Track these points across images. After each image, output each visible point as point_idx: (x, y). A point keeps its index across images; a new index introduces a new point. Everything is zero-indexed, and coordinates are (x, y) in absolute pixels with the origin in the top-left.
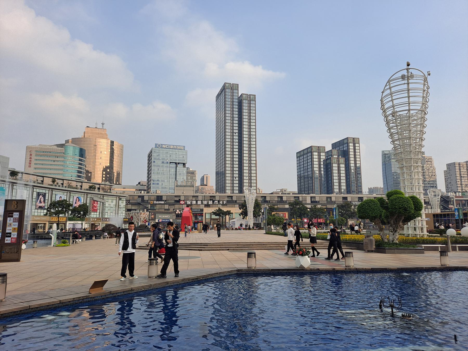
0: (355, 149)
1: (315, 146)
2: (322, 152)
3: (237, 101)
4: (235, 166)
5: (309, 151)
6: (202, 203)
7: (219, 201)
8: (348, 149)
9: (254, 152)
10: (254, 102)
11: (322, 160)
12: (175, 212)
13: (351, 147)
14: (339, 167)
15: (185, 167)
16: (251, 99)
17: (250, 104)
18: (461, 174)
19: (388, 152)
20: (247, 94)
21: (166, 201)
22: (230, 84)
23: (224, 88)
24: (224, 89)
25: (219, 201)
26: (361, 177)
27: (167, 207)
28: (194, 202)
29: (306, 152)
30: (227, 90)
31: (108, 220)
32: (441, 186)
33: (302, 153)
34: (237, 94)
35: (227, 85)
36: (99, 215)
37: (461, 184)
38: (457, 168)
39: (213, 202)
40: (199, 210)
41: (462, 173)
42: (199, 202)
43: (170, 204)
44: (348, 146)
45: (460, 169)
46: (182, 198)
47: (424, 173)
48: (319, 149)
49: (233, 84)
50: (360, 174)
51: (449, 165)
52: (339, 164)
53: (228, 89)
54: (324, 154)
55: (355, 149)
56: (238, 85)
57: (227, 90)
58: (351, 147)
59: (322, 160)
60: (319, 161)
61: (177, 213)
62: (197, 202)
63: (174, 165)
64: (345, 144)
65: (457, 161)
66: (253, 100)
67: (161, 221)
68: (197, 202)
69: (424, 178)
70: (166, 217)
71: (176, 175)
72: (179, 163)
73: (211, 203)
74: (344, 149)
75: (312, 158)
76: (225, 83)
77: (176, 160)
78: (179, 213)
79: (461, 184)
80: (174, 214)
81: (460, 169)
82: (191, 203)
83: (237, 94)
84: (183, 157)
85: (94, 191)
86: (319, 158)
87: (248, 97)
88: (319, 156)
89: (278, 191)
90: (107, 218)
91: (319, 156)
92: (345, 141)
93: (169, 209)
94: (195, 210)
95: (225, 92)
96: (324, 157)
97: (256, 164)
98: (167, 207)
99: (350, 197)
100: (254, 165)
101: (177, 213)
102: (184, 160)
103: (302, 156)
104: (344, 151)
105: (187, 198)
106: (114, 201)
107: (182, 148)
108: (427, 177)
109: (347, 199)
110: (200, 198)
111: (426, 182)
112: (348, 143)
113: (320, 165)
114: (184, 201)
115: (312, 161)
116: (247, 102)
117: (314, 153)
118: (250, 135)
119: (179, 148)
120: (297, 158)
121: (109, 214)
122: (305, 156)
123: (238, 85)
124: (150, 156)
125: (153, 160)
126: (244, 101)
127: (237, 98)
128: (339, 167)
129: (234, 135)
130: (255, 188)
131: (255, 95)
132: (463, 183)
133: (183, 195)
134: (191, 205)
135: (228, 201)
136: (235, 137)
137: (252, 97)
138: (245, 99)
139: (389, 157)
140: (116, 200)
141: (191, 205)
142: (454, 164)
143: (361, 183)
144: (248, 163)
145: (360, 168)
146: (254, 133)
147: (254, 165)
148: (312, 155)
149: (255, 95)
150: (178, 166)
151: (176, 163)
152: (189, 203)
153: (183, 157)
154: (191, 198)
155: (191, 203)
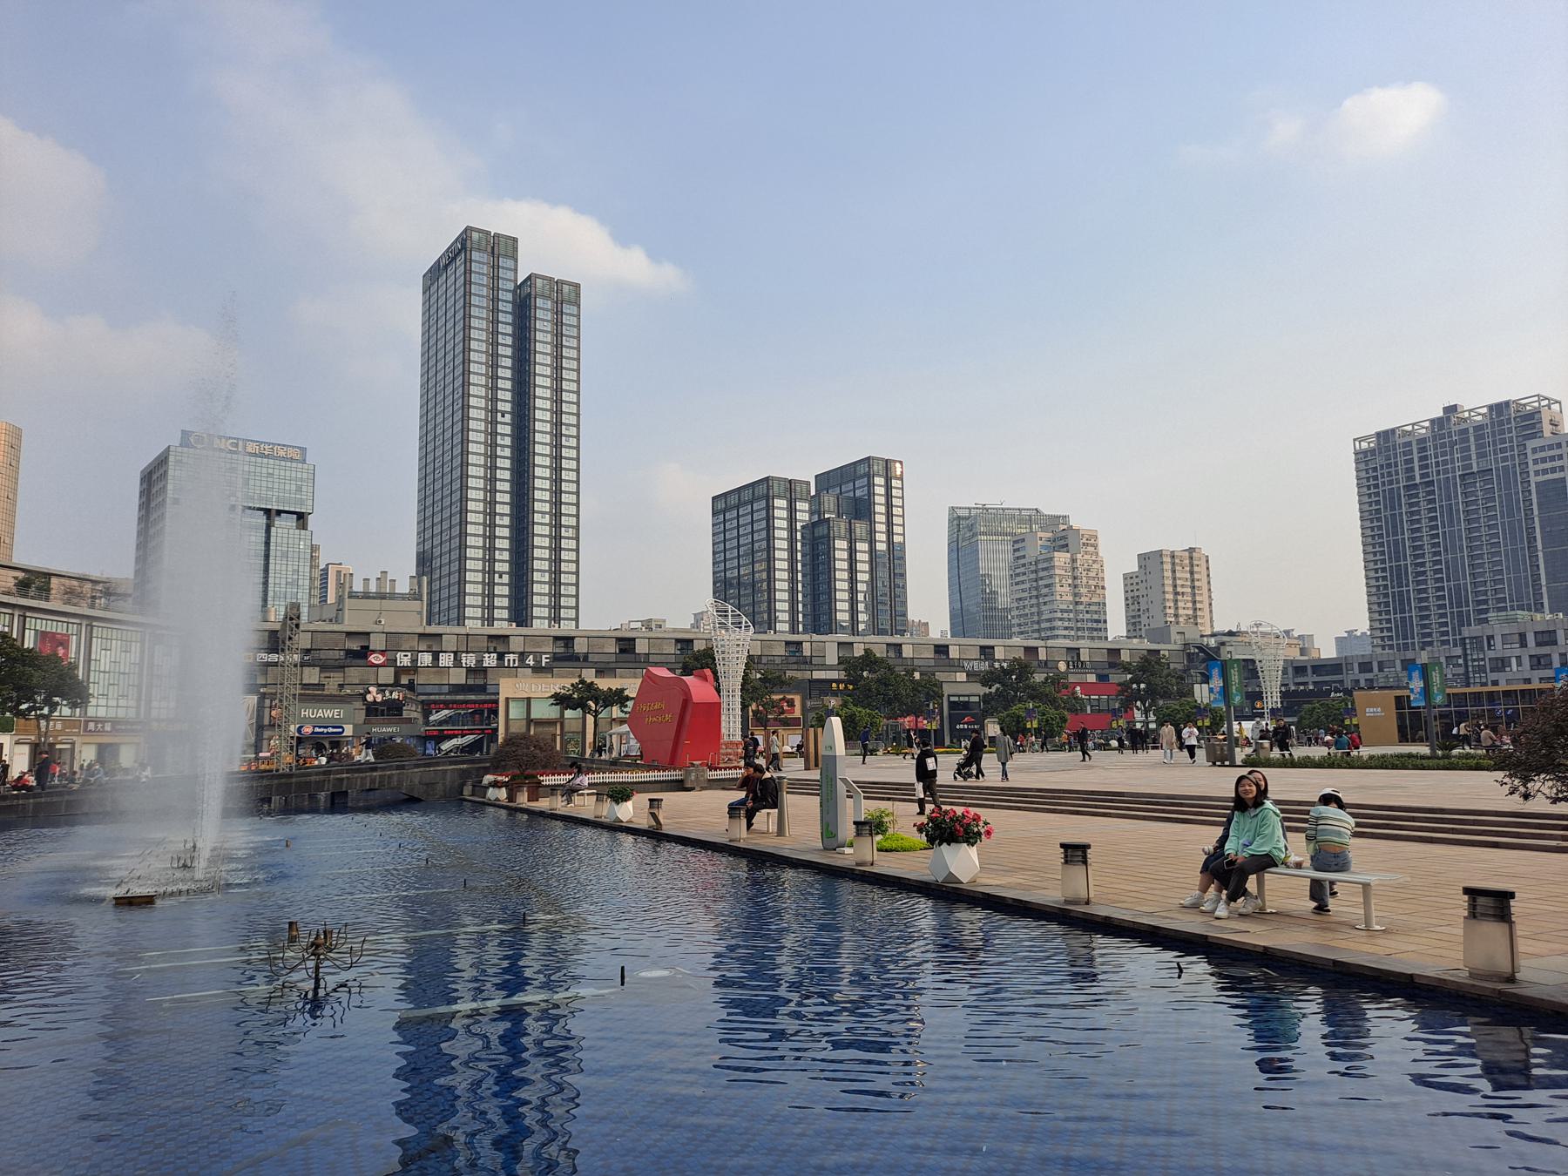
0: (888, 496)
1: (779, 479)
2: (801, 500)
3: (509, 297)
4: (498, 531)
5: (759, 493)
6: (457, 663)
7: (522, 656)
8: (871, 494)
9: (573, 487)
10: (574, 310)
11: (799, 525)
12: (363, 696)
13: (880, 490)
14: (852, 551)
15: (304, 527)
16: (565, 295)
17: (559, 313)
18: (1175, 586)
19: (965, 513)
20: (551, 279)
21: (308, 651)
22: (488, 233)
23: (464, 247)
24: (463, 246)
25: (522, 656)
26: (904, 587)
27: (312, 675)
28: (426, 659)
29: (746, 496)
30: (469, 260)
31: (108, 727)
32: (1117, 626)
33: (733, 500)
34: (510, 275)
35: (475, 236)
36: (138, 707)
37: (1176, 616)
38: (1168, 567)
39: (501, 657)
40: (446, 689)
41: (1179, 582)
42: (446, 660)
43: (325, 667)
44: (870, 485)
45: (1174, 572)
46: (377, 642)
47: (1075, 578)
48: (791, 489)
49: (497, 236)
50: (903, 575)
51: (1144, 558)
52: (852, 543)
53: (479, 250)
54: (806, 506)
55: (888, 496)
56: (515, 240)
57: (469, 260)
58: (880, 490)
59: (799, 525)
60: (792, 529)
61: (369, 698)
62: (436, 658)
63: (262, 519)
64: (862, 477)
65: (1101, 542)
66: (570, 303)
67: (308, 730)
68: (436, 658)
69: (1075, 595)
70: (328, 713)
71: (267, 557)
72: (279, 512)
73: (494, 664)
74: (858, 493)
75: (770, 518)
76: (468, 230)
77: (267, 500)
78: (379, 698)
79: (1176, 616)
80: (359, 704)
81: (1174, 572)
82: (414, 661)
83: (510, 275)
84: (299, 489)
85: (47, 599)
86: (792, 519)
87: (551, 289)
88: (792, 510)
89: (633, 625)
90: (103, 721)
91: (792, 510)
92: (862, 469)
93: (320, 686)
94: (429, 689)
95: (468, 261)
96: (806, 517)
97: (577, 528)
98: (312, 675)
99: (809, 643)
100: (571, 533)
101: (369, 698)
102: (302, 502)
103: (731, 508)
104: (856, 500)
105: (395, 641)
106: (135, 648)
107: (291, 453)
108: (1083, 591)
109: (947, 653)
110: (449, 643)
111: (1081, 607)
112: (869, 477)
113: (792, 540)
114: (382, 652)
115: (770, 528)
116: (549, 304)
117: (777, 503)
118: (557, 424)
119: (282, 453)
120: (714, 514)
121: (112, 703)
122: (742, 510)
123: (515, 240)
124: (153, 478)
125: (170, 493)
126: (539, 302)
127: (511, 286)
128: (852, 551)
129: (499, 418)
130: (572, 613)
131: (577, 286)
132: (1181, 612)
133: (378, 628)
134: (414, 668)
135: (556, 658)
136: (500, 429)
137: (566, 288)
138: (543, 296)
139: (971, 528)
140: (142, 642)
141: (414, 668)
142: (1160, 553)
143: (904, 603)
144: (550, 524)
145: (903, 550)
146: (573, 420)
147: (571, 533)
148: (769, 508)
149: (577, 286)
150: (278, 522)
151: (267, 512)
152: (404, 660)
153: (299, 489)
154: (414, 643)
155: (414, 661)
